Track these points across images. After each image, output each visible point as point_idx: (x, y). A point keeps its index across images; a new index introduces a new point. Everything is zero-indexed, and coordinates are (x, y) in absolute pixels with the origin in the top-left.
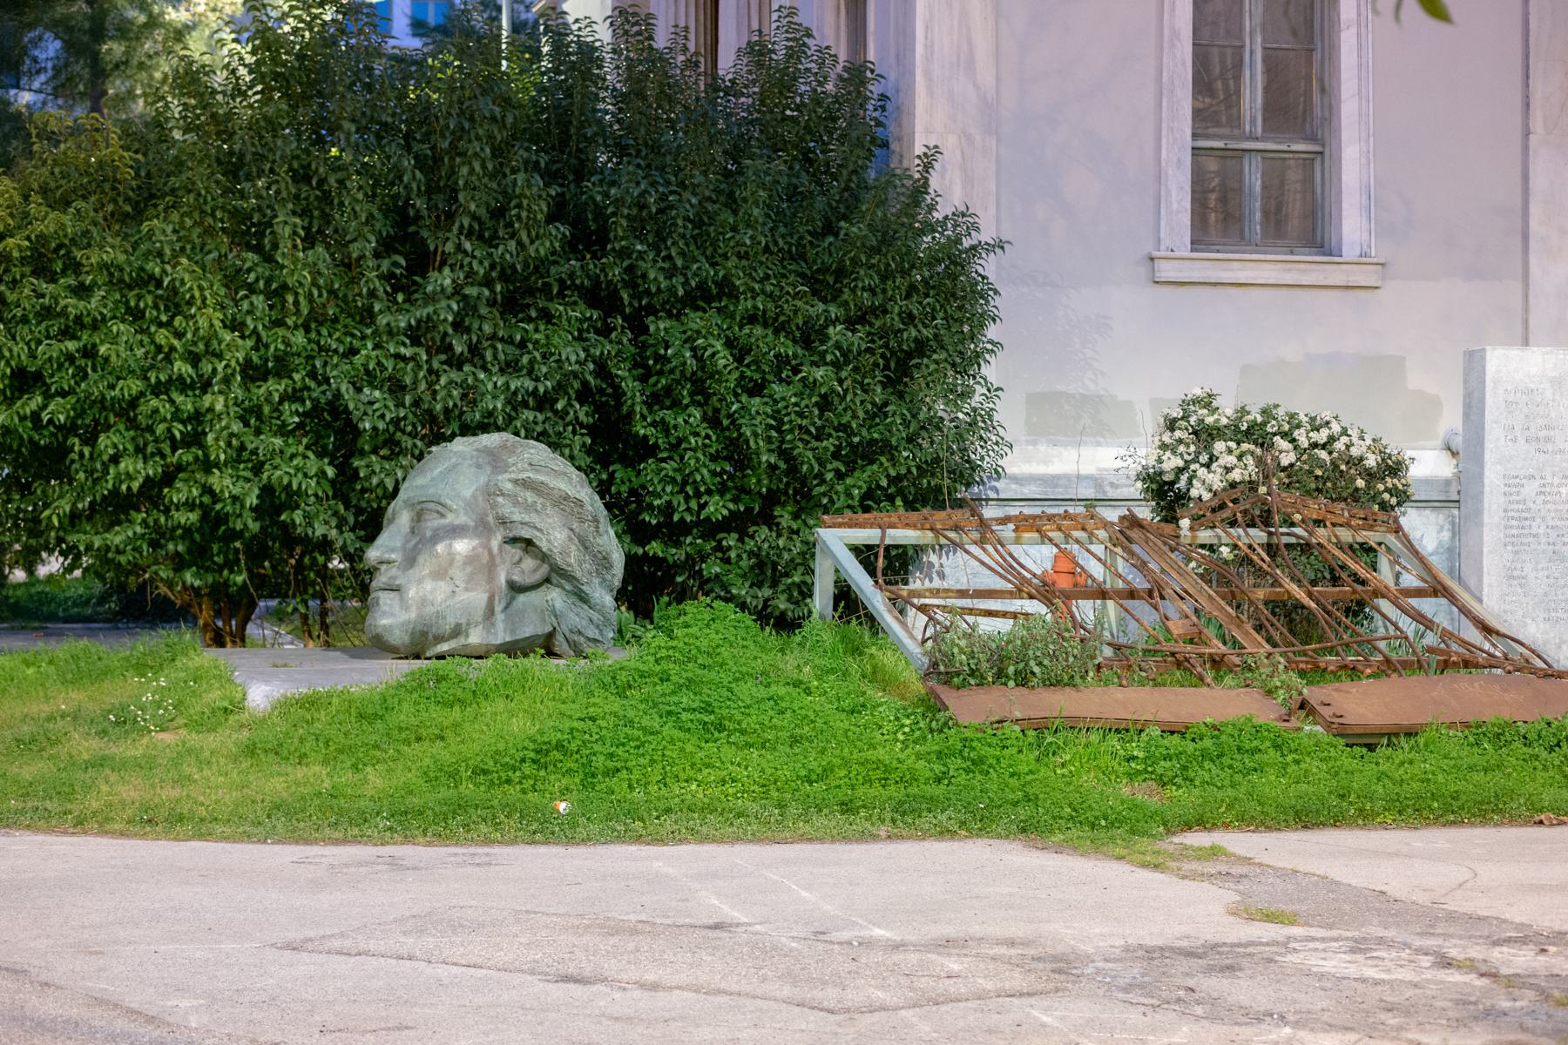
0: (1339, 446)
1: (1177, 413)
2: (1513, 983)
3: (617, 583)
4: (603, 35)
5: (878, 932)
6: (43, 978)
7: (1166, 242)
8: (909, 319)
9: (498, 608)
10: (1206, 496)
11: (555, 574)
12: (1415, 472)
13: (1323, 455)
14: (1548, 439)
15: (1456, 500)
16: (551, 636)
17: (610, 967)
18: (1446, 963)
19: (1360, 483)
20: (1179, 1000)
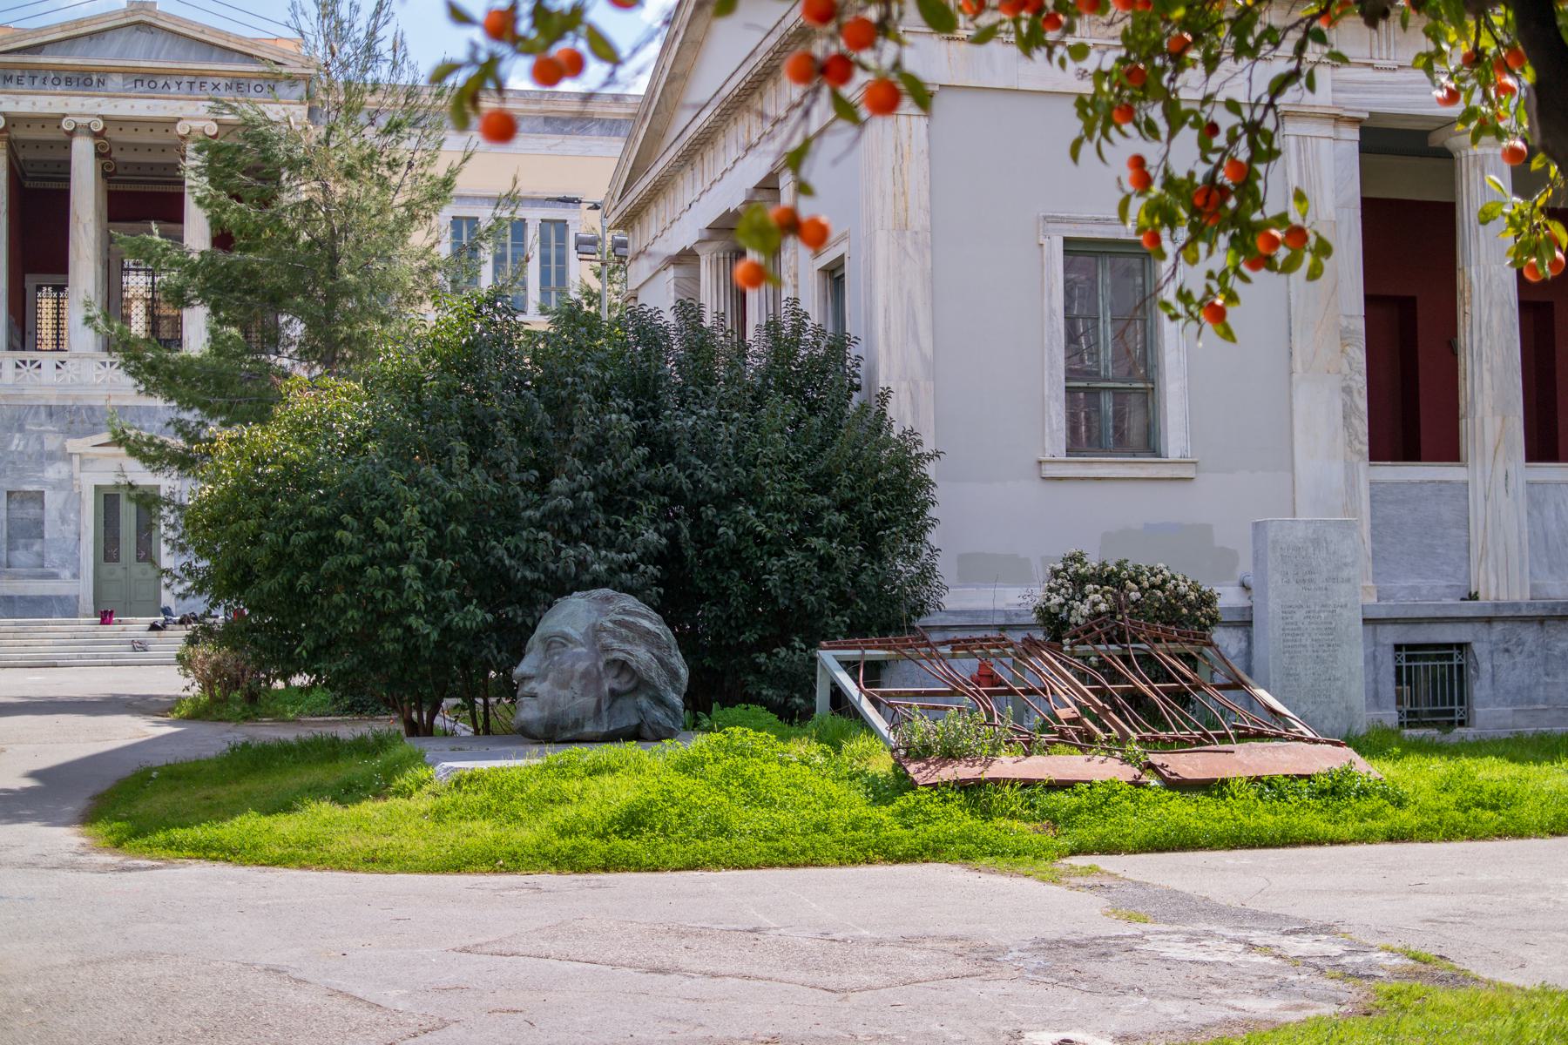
0: (1170, 586)
1: (1060, 566)
2: (1299, 962)
3: (684, 690)
4: (669, 317)
5: (865, 932)
6: (297, 975)
7: (1049, 451)
8: (878, 505)
9: (604, 707)
10: (1081, 621)
11: (641, 684)
12: (1221, 603)
13: (1159, 593)
14: (1311, 581)
15: (1244, 623)
16: (639, 726)
17: (684, 960)
18: (1251, 947)
19: (1185, 611)
20: (1070, 979)
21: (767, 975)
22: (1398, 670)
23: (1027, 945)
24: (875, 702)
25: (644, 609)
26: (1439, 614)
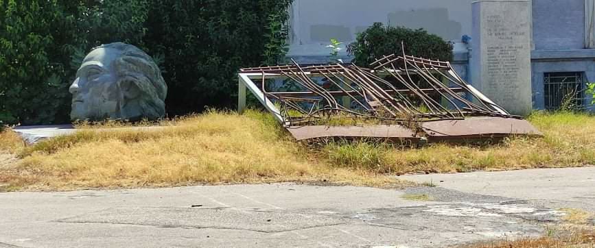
9: (121, 106)
11: (141, 94)
12: (454, 50)
21: (229, 226)
22: (546, 87)
23: (365, 211)
24: (270, 98)
25: (142, 53)
26: (478, 154)
